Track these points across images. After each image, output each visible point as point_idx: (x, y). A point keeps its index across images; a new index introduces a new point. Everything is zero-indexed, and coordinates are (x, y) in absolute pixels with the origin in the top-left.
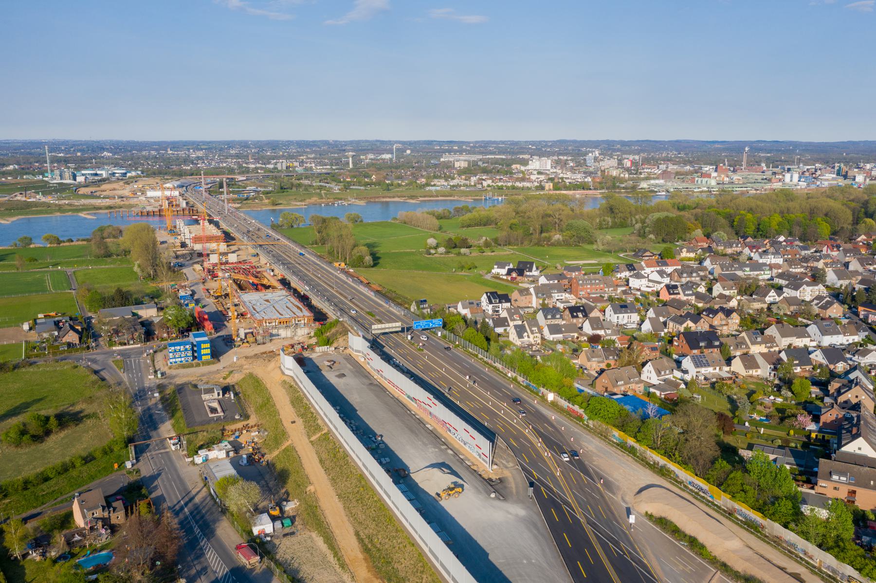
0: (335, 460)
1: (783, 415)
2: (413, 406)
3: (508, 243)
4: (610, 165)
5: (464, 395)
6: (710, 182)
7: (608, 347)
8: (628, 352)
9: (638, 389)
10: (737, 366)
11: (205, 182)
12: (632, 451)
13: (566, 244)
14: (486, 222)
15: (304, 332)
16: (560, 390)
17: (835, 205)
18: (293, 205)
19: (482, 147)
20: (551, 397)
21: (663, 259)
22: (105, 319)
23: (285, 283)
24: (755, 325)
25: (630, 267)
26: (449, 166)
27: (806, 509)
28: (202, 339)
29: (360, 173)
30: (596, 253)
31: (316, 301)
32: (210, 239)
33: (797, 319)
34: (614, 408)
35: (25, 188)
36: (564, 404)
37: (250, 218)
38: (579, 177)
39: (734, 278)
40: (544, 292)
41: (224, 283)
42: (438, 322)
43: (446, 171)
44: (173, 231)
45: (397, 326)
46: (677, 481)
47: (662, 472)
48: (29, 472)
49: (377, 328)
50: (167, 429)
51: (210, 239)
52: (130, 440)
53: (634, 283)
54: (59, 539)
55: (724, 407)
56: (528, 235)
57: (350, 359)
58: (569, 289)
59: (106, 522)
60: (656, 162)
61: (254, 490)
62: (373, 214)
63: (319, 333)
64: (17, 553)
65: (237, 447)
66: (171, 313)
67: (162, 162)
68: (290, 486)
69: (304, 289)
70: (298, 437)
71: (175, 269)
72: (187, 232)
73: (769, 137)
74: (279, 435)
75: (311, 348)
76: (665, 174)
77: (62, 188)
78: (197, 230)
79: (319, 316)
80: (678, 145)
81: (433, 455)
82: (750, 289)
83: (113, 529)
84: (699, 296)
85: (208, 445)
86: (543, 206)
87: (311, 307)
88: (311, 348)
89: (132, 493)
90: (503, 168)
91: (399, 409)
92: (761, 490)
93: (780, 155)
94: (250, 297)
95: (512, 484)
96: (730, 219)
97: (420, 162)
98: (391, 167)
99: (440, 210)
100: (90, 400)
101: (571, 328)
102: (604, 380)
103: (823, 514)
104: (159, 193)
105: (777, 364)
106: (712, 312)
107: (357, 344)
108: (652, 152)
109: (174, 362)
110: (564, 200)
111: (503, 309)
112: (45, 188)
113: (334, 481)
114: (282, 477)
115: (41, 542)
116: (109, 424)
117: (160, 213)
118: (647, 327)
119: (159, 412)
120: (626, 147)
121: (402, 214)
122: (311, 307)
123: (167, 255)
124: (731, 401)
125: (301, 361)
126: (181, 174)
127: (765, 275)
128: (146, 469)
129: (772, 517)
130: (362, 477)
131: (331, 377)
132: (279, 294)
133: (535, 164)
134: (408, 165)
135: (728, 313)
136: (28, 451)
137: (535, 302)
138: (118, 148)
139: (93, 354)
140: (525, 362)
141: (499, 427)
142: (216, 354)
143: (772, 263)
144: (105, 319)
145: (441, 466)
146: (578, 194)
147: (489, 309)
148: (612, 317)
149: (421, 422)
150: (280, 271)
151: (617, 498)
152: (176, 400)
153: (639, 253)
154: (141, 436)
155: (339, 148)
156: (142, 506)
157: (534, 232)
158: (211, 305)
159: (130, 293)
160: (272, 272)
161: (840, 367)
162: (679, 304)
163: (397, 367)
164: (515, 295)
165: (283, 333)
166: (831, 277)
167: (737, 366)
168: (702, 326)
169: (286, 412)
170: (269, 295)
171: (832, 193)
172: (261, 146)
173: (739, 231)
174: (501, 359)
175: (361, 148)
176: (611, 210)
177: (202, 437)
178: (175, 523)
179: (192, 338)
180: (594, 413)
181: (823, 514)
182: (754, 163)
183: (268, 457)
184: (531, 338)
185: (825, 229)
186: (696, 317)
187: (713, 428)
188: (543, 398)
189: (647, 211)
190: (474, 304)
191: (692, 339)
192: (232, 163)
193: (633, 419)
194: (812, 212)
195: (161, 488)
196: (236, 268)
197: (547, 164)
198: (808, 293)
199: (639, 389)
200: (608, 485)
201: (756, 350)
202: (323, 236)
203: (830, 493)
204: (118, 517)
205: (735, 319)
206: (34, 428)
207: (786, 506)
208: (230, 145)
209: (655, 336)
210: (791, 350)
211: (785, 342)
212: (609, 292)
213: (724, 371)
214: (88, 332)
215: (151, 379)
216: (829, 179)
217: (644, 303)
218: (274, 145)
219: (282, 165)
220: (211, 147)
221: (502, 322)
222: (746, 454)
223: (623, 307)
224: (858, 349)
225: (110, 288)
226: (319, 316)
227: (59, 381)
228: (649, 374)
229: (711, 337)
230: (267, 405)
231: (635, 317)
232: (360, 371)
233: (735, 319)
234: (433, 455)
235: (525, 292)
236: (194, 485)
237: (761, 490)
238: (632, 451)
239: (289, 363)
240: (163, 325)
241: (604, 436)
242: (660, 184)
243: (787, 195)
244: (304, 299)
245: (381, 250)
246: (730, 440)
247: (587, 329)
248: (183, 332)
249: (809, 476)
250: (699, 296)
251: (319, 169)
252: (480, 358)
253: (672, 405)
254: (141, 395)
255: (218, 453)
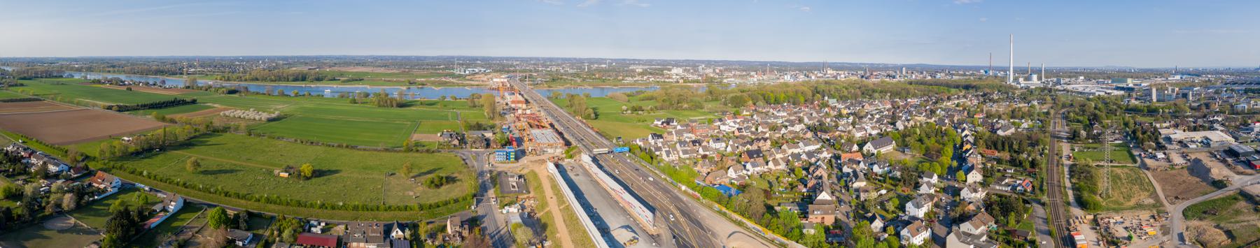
0: (571, 220)
1: (792, 186)
2: (613, 193)
3: (662, 109)
4: (709, 71)
5: (640, 188)
6: (754, 79)
7: (711, 160)
8: (720, 163)
9: (726, 181)
10: (771, 165)
11: (519, 75)
12: (725, 214)
13: (690, 109)
14: (651, 98)
15: (559, 151)
16: (688, 184)
17: (805, 89)
18: (559, 88)
19: (650, 62)
20: (684, 188)
21: (735, 115)
22: (471, 135)
23: (552, 125)
24: (777, 145)
25: (720, 120)
26: (633, 71)
27: (805, 231)
28: (511, 150)
29: (591, 73)
30: (704, 114)
31: (566, 136)
32: (519, 102)
33: (794, 140)
34: (715, 192)
35: (446, 76)
36: (690, 191)
37: (539, 94)
38: (695, 77)
39: (767, 123)
40: (679, 133)
41: (523, 123)
42: (627, 149)
43: (632, 73)
44: (503, 98)
45: (606, 150)
46: (747, 228)
47: (740, 224)
48: (432, 201)
49: (596, 151)
50: (491, 193)
51: (519, 102)
52: (475, 196)
53: (722, 128)
54: (440, 236)
55: (766, 186)
56: (672, 104)
57: (582, 166)
58: (692, 131)
59: (460, 234)
60: (730, 70)
61: (530, 232)
62: (596, 94)
63: (567, 152)
64: (423, 238)
65: (523, 208)
66: (499, 135)
67: (501, 66)
68: (548, 233)
69: (561, 129)
70: (553, 206)
71: (502, 115)
72: (509, 98)
73: (777, 60)
74: (544, 204)
75: (562, 159)
76: (734, 76)
77: (460, 76)
78: (513, 98)
79: (568, 143)
80: (740, 63)
81: (623, 221)
82: (774, 128)
83: (463, 238)
84: (752, 133)
85: (509, 204)
86: (678, 91)
87: (564, 138)
88: (562, 159)
89: (473, 222)
90: (659, 72)
91: (605, 194)
92: (785, 225)
93: (782, 68)
94: (535, 132)
95: (664, 237)
96: (763, 95)
97: (620, 69)
98: (605, 71)
99: (629, 92)
100: (460, 172)
101: (693, 151)
102: (709, 178)
103: (812, 231)
104: (499, 80)
105: (788, 162)
106: (758, 140)
107: (586, 159)
108: (728, 66)
109: (497, 160)
110: (689, 88)
111: (660, 142)
112: (453, 76)
113: (570, 232)
114: (544, 227)
115: (433, 236)
116: (466, 186)
117: (498, 89)
118: (729, 149)
119: (489, 183)
120: (717, 63)
121: (610, 94)
122: (564, 138)
123: (499, 109)
124: (770, 183)
125: (557, 166)
126: (508, 72)
127: (780, 121)
128: (481, 212)
129: (791, 238)
130: (585, 231)
131: (572, 175)
132: (549, 131)
133: (675, 71)
134: (614, 70)
135: (765, 140)
136: (433, 191)
137: (675, 138)
138: (484, 59)
139: (463, 151)
140: (671, 170)
141: (656, 205)
142: (517, 159)
143: (781, 115)
144: (471, 135)
145: (627, 227)
146: (695, 85)
147: (652, 142)
148: (713, 145)
149: (617, 202)
150: (550, 120)
151: (718, 241)
152: (497, 179)
153: (724, 113)
154: (479, 195)
155: (581, 61)
156: (476, 230)
157: (675, 103)
158: (517, 134)
159: (483, 128)
160: (546, 119)
161: (813, 160)
162: (743, 137)
163: (605, 172)
164: (665, 135)
165: (550, 151)
166: (806, 120)
167: (771, 165)
168: (754, 147)
169: (549, 192)
170: (544, 131)
171: (803, 84)
172: (545, 60)
173: (768, 102)
174: (659, 168)
175: (591, 61)
176: (711, 93)
177: (507, 200)
178: (490, 242)
179: (507, 149)
180: (706, 196)
181: (812, 231)
182: (772, 71)
183: (538, 215)
184: (673, 157)
185: (802, 99)
186: (751, 143)
187: (762, 198)
188: (680, 189)
189: (727, 93)
190: (645, 140)
191: (751, 154)
192: (531, 67)
193: (723, 197)
194: (797, 92)
195: (486, 223)
196: (529, 117)
197: (680, 71)
198: (798, 128)
199: (727, 181)
200: (714, 234)
201: (779, 156)
202: (571, 103)
203: (815, 221)
204: (465, 233)
205: (769, 142)
206: (437, 182)
207: (797, 231)
208: (531, 59)
209: (733, 153)
210: (793, 155)
211: (790, 152)
212: (711, 132)
213: (765, 169)
214: (463, 141)
215: (487, 167)
216: (802, 78)
217: (727, 137)
218: (551, 60)
219: (554, 69)
220: (523, 60)
221: (659, 149)
222: (777, 208)
223: (718, 140)
224: (819, 151)
225: (473, 121)
226: (568, 143)
227: (449, 161)
228: (731, 173)
229: (758, 152)
230: (539, 187)
231: (724, 145)
232: (587, 173)
233: (769, 142)
234: (623, 221)
235: (670, 133)
236: (501, 225)
237: (785, 225)
238: (725, 214)
239: (551, 166)
240: (495, 141)
241: (711, 208)
242: (732, 80)
243: (786, 85)
244: (561, 134)
245: (599, 111)
246: (770, 202)
247: (701, 152)
248: (504, 146)
249: (804, 214)
250: (752, 133)
251: (571, 71)
252: (646, 166)
253: (743, 188)
254: (481, 174)
255: (514, 209)
